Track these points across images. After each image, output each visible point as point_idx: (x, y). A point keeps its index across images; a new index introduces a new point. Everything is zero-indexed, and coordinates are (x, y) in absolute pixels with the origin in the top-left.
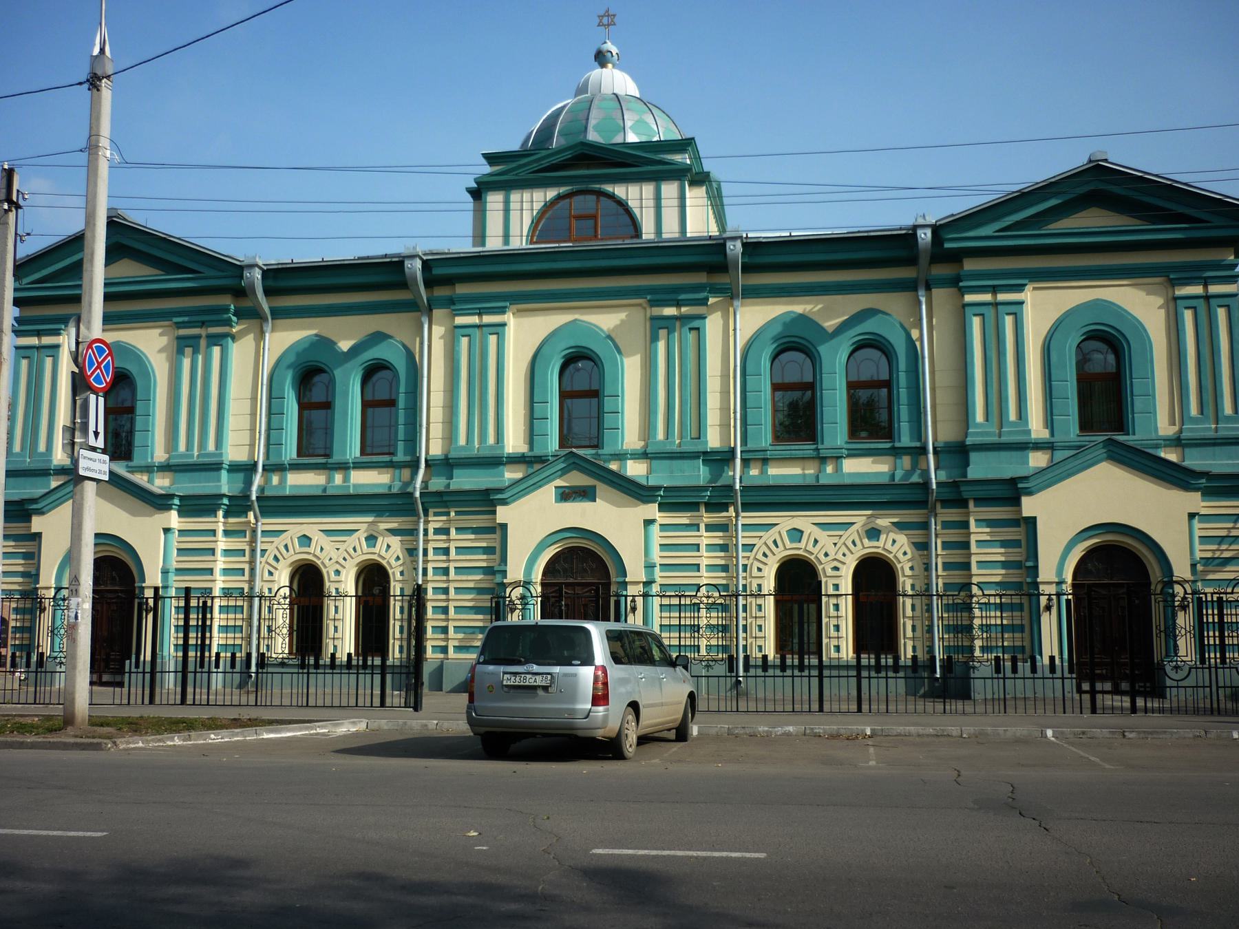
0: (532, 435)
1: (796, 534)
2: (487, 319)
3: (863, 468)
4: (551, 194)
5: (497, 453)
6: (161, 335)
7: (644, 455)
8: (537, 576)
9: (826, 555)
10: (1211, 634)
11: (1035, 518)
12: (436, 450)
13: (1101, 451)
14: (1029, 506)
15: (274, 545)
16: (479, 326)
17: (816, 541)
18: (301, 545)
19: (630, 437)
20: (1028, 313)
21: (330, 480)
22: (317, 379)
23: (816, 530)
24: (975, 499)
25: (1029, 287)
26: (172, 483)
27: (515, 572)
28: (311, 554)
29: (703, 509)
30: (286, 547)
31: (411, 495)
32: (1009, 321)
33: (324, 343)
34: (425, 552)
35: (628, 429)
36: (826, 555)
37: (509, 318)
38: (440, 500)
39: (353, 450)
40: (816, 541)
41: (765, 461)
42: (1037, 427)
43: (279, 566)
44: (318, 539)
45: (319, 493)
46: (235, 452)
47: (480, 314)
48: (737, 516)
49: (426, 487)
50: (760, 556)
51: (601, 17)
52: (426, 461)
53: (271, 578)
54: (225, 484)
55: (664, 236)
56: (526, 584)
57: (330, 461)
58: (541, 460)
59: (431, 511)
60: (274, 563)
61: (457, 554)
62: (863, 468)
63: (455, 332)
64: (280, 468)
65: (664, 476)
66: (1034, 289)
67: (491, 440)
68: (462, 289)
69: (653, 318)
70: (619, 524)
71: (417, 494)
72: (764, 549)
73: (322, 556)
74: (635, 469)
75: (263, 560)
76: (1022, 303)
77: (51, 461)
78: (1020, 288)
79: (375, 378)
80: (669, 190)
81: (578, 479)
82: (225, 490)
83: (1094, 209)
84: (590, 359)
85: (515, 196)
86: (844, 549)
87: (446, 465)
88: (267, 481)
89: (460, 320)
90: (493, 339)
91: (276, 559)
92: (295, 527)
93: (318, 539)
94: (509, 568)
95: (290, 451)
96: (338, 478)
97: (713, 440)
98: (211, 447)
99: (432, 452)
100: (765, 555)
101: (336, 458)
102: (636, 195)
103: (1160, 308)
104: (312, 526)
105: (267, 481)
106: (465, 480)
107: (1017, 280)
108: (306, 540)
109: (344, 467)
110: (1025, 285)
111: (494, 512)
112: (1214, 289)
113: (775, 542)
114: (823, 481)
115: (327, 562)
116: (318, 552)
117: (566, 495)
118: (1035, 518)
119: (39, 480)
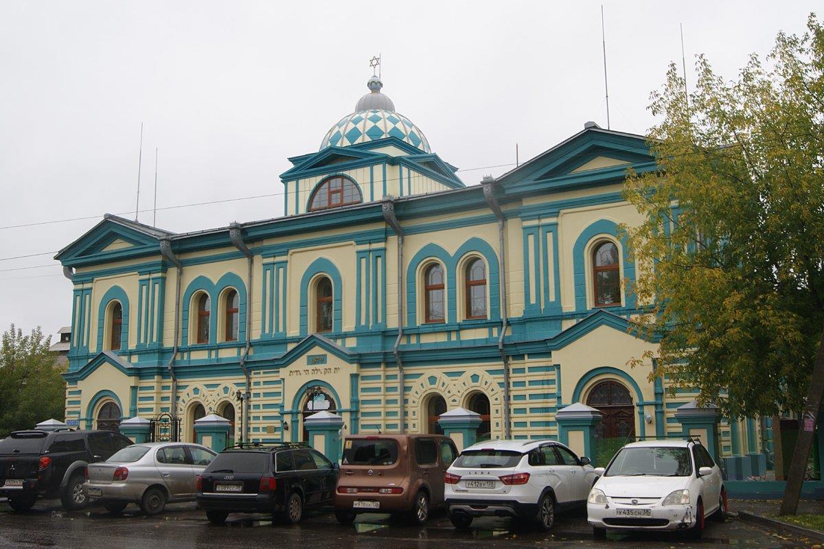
0: (303, 325)
1: (432, 380)
2: (278, 259)
4: (319, 178)
19: (348, 325)
22: (434, 269)
24: (528, 354)
26: (139, 360)
28: (438, 389)
32: (550, 236)
33: (117, 290)
41: (418, 335)
42: (569, 306)
47: (539, 219)
51: (371, 61)
55: (375, 200)
60: (450, 395)
62: (228, 354)
63: (528, 231)
68: (266, 243)
69: (524, 228)
76: (287, 262)
77: (561, 308)
79: (473, 267)
80: (378, 169)
83: (600, 158)
84: (611, 242)
85: (301, 182)
90: (550, 236)
93: (204, 390)
95: (192, 341)
98: (281, 330)
102: (360, 175)
104: (437, 371)
107: (555, 210)
109: (219, 347)
119: (281, 347)
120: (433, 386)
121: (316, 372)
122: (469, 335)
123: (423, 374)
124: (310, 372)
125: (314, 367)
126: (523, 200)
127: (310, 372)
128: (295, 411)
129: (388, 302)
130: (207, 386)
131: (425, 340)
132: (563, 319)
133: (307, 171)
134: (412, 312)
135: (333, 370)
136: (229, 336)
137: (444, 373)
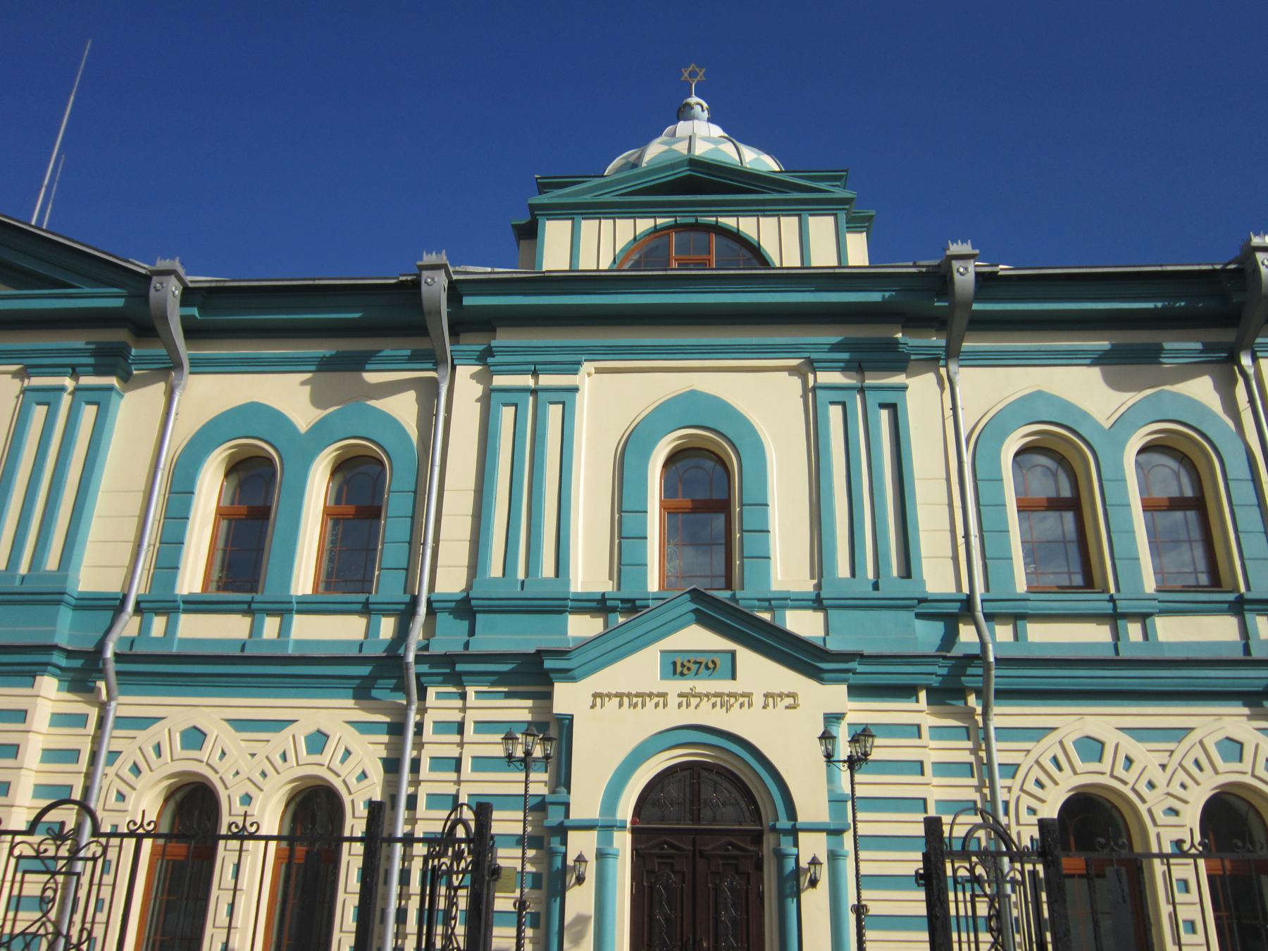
1: (1092, 747)
2: (546, 380)
3: (344, 630)
5: (556, 591)
6: (303, 383)
7: (817, 603)
8: (625, 810)
9: (1151, 785)
10: (964, 936)
11: (571, 718)
12: (451, 582)
13: (692, 616)
14: (566, 698)
15: (137, 743)
16: (534, 392)
17: (348, 752)
18: (184, 747)
20: (583, 402)
21: (255, 630)
23: (1125, 740)
25: (588, 367)
27: (585, 800)
29: (923, 695)
30: (158, 750)
31: (402, 659)
34: (416, 764)
35: (785, 564)
36: (1151, 785)
37: (587, 379)
38: (452, 670)
39: (303, 581)
40: (348, 752)
43: (140, 783)
44: (219, 733)
45: (354, 652)
46: (95, 573)
48: (985, 714)
49: (426, 647)
50: (1030, 786)
52: (429, 602)
53: (120, 805)
54: (65, 629)
56: (606, 828)
57: (258, 597)
58: (632, 606)
59: (431, 692)
60: (130, 777)
61: (474, 769)
62: (344, 630)
64: (170, 607)
65: (849, 635)
66: (599, 371)
67: (547, 569)
70: (782, 721)
71: (411, 658)
72: (1037, 772)
73: (222, 767)
74: (805, 624)
75: (111, 771)
76: (575, 390)
78: (573, 368)
81: (697, 638)
82: (62, 639)
86: (1181, 776)
87: (465, 608)
88: (144, 628)
89: (499, 381)
90: (554, 412)
91: (136, 770)
92: (178, 711)
94: (574, 799)
95: (192, 577)
96: (271, 627)
97: (937, 579)
98: (52, 563)
99: (439, 589)
100: (1039, 783)
101: (269, 591)
103: (477, 401)
104: (211, 712)
105: (144, 628)
106: (500, 636)
108: (194, 738)
109: (284, 609)
110: (579, 363)
111: (549, 696)
112: (546, 380)
113: (1197, 763)
114: (1125, 654)
115: (229, 778)
116: (215, 760)
117: (678, 666)
118: (571, 718)
120: (316, 758)
121: (694, 701)
122: (1174, 632)
123: (1192, 729)
124: (673, 700)
125: (685, 685)
126: (498, 330)
127: (673, 700)
128: (608, 819)
129: (468, 522)
130: (239, 725)
131: (1041, 634)
132: (786, 607)
133: (822, 185)
134: (172, 543)
135: (758, 700)
136: (349, 571)
137: (231, 722)
